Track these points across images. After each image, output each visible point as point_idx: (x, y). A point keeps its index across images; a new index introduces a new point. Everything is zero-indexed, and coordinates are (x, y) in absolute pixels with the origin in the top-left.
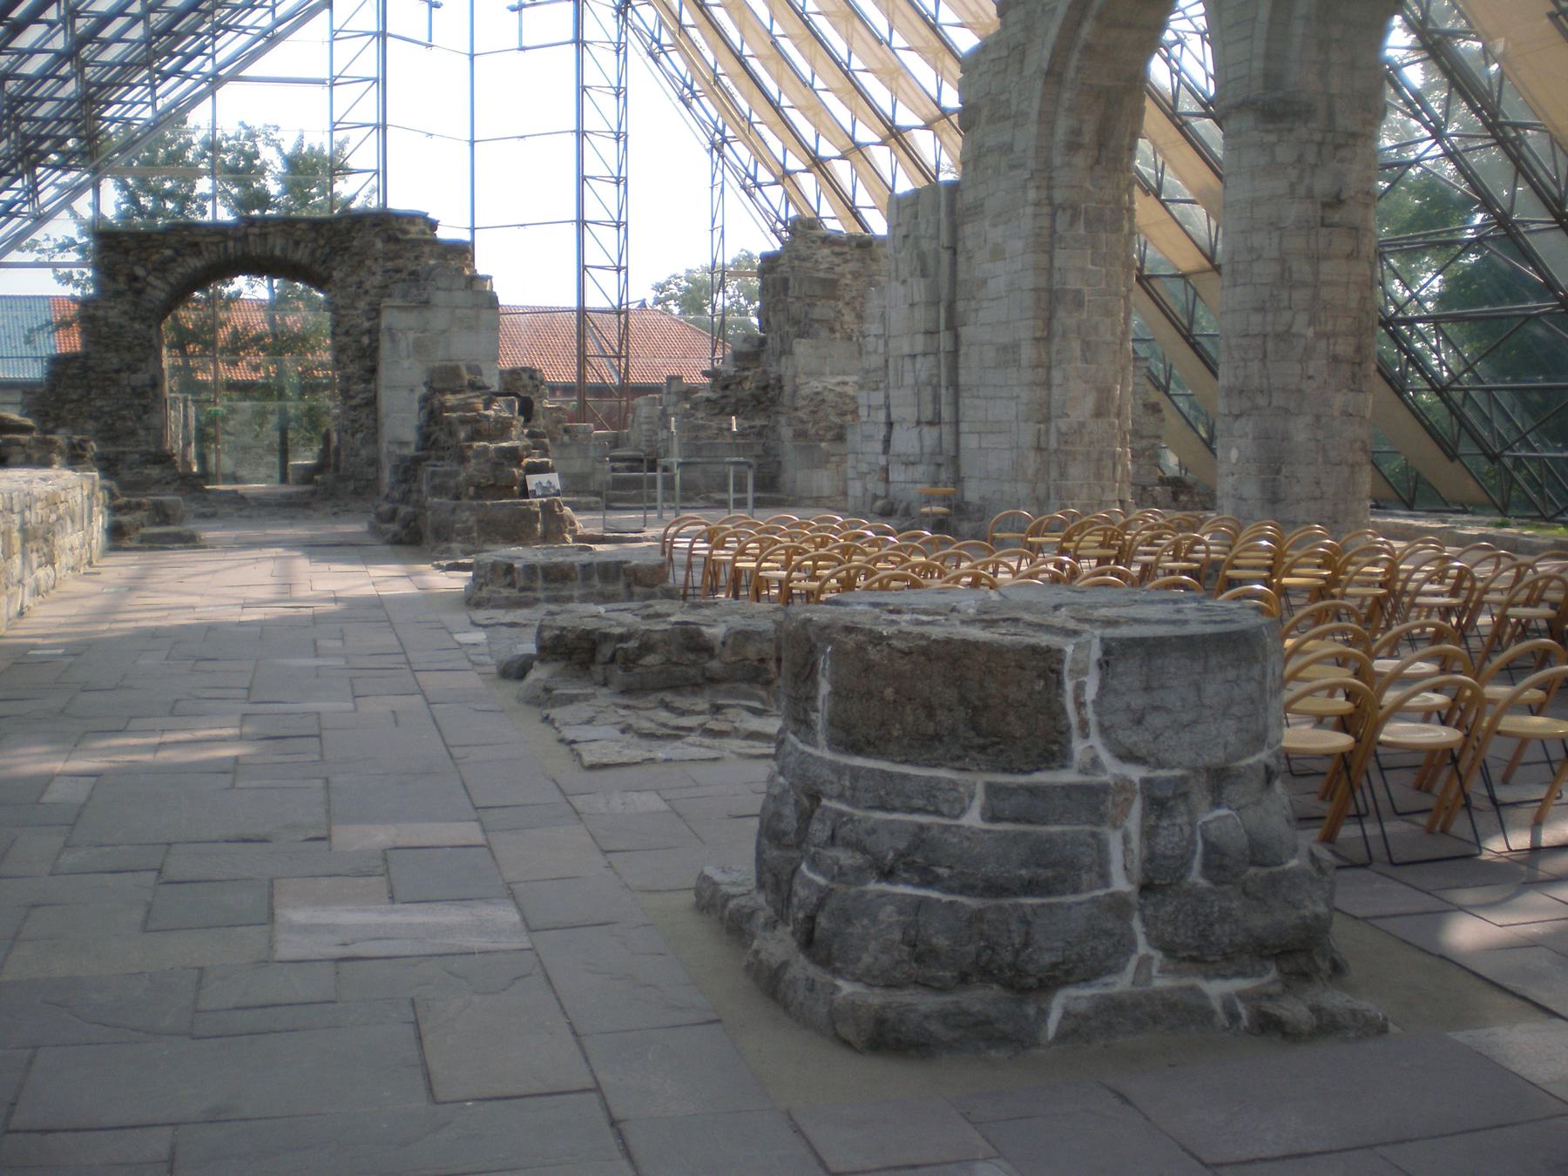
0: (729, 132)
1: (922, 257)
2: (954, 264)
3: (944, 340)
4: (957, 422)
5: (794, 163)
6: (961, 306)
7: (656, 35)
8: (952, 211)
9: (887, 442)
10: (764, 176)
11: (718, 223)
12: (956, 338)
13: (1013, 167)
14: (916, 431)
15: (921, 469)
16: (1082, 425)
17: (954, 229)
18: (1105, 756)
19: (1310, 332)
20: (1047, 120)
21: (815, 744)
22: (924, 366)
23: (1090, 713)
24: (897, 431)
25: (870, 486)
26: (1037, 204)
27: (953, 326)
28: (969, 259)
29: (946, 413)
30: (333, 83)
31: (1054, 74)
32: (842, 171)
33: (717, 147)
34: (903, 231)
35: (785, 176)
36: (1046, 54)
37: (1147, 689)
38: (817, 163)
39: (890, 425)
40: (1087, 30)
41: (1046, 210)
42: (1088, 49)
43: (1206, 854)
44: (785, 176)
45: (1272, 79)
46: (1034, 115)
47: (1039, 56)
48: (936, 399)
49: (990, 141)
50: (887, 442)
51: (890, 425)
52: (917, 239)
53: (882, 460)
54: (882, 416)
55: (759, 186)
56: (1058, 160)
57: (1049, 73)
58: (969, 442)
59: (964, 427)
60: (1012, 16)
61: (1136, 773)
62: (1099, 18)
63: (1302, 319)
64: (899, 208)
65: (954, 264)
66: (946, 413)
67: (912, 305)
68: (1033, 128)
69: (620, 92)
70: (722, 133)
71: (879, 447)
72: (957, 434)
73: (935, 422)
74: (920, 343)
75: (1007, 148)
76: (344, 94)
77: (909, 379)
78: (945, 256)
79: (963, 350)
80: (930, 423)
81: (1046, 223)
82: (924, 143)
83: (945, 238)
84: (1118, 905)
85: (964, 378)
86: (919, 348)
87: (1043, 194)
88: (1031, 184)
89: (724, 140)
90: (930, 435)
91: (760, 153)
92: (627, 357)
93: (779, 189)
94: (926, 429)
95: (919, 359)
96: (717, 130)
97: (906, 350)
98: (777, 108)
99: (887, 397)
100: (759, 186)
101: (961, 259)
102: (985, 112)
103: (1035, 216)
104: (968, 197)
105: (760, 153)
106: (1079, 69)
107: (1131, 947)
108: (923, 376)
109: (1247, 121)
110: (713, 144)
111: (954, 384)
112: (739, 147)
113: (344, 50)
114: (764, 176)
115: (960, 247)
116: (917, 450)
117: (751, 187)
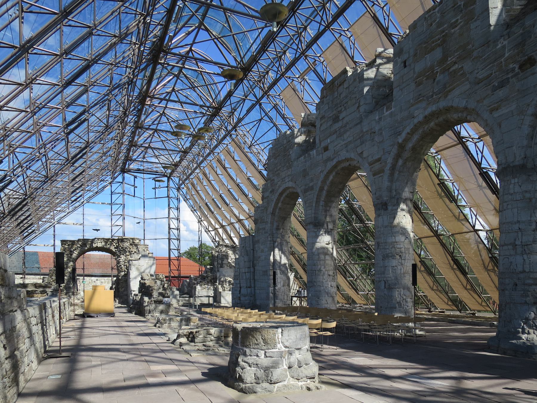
0: (202, 219)
1: (247, 251)
2: (253, 253)
3: (252, 270)
4: (255, 287)
5: (217, 226)
6: (255, 262)
7: (215, 238)
8: (253, 242)
9: (240, 291)
10: (210, 229)
11: (200, 239)
12: (254, 269)
13: (265, 233)
14: (246, 289)
15: (247, 297)
16: (280, 288)
17: (254, 245)
18: (283, 347)
19: (324, 270)
20: (272, 223)
21: (238, 346)
22: (248, 275)
23: (280, 340)
24: (242, 289)
25: (236, 301)
26: (270, 241)
27: (254, 266)
28: (257, 252)
29: (252, 285)
30: (111, 204)
31: (273, 214)
32: (228, 228)
33: (200, 222)
34: (243, 245)
35: (215, 229)
36: (272, 209)
37: (288, 336)
38: (222, 227)
39: (241, 288)
40: (280, 205)
41: (272, 242)
42: (280, 208)
43: (298, 362)
44: (215, 229)
45: (316, 218)
46: (269, 222)
47: (270, 209)
48: (250, 282)
49: (261, 227)
50: (240, 291)
51: (241, 288)
52: (246, 247)
53: (239, 295)
54: (239, 285)
55: (195, 210)
56: (274, 232)
57: (272, 213)
58: (257, 291)
59: (256, 288)
60: (265, 201)
61: (287, 349)
62: (282, 202)
63: (323, 267)
64: (241, 239)
65: (253, 253)
66: (252, 285)
67: (245, 262)
68: (269, 225)
69: (178, 209)
70: (201, 219)
71: (238, 292)
72: (255, 290)
73: (250, 287)
74: (247, 270)
75: (264, 229)
76: (115, 207)
77: (244, 278)
78: (252, 251)
79: (256, 272)
80: (249, 287)
81: (272, 245)
82: (246, 223)
83: (251, 248)
84: (285, 369)
85: (256, 278)
86: (246, 271)
87: (271, 239)
88: (269, 237)
89: (201, 221)
90: (249, 290)
91: (210, 223)
92: (180, 270)
93: (214, 232)
94: (248, 289)
95: (247, 273)
96: (200, 218)
97: (244, 271)
98: (213, 213)
99: (240, 281)
100: (209, 231)
101: (255, 252)
102: (259, 221)
103: (270, 244)
104: (256, 239)
105: (210, 223)
106: (278, 213)
107: (287, 377)
108: (247, 277)
109: (311, 226)
110: (199, 221)
111: (254, 279)
112: (205, 222)
113: (115, 197)
114: (210, 229)
115: (255, 250)
116: (246, 293)
117: (208, 231)
